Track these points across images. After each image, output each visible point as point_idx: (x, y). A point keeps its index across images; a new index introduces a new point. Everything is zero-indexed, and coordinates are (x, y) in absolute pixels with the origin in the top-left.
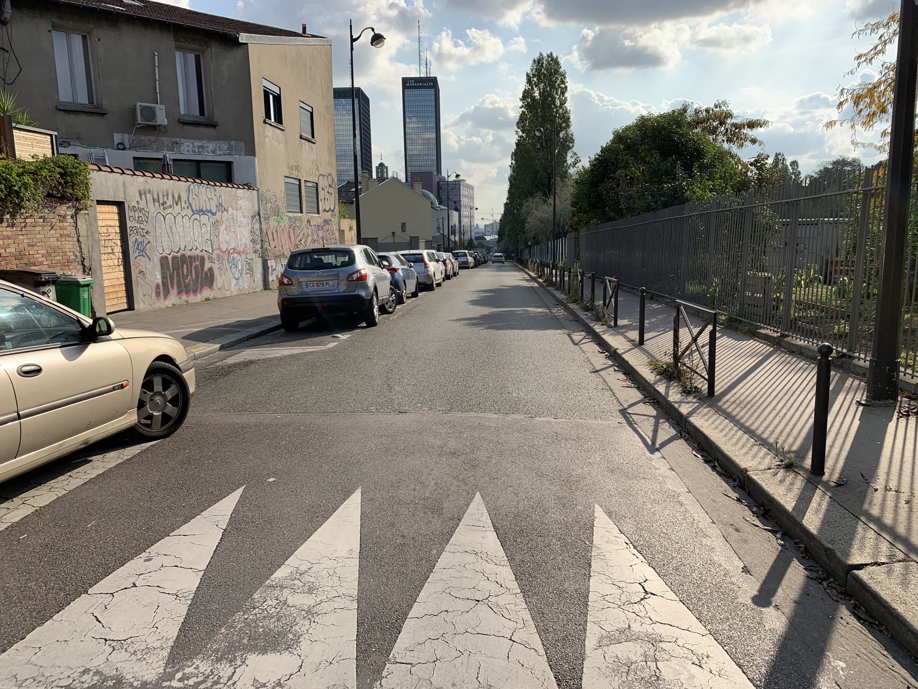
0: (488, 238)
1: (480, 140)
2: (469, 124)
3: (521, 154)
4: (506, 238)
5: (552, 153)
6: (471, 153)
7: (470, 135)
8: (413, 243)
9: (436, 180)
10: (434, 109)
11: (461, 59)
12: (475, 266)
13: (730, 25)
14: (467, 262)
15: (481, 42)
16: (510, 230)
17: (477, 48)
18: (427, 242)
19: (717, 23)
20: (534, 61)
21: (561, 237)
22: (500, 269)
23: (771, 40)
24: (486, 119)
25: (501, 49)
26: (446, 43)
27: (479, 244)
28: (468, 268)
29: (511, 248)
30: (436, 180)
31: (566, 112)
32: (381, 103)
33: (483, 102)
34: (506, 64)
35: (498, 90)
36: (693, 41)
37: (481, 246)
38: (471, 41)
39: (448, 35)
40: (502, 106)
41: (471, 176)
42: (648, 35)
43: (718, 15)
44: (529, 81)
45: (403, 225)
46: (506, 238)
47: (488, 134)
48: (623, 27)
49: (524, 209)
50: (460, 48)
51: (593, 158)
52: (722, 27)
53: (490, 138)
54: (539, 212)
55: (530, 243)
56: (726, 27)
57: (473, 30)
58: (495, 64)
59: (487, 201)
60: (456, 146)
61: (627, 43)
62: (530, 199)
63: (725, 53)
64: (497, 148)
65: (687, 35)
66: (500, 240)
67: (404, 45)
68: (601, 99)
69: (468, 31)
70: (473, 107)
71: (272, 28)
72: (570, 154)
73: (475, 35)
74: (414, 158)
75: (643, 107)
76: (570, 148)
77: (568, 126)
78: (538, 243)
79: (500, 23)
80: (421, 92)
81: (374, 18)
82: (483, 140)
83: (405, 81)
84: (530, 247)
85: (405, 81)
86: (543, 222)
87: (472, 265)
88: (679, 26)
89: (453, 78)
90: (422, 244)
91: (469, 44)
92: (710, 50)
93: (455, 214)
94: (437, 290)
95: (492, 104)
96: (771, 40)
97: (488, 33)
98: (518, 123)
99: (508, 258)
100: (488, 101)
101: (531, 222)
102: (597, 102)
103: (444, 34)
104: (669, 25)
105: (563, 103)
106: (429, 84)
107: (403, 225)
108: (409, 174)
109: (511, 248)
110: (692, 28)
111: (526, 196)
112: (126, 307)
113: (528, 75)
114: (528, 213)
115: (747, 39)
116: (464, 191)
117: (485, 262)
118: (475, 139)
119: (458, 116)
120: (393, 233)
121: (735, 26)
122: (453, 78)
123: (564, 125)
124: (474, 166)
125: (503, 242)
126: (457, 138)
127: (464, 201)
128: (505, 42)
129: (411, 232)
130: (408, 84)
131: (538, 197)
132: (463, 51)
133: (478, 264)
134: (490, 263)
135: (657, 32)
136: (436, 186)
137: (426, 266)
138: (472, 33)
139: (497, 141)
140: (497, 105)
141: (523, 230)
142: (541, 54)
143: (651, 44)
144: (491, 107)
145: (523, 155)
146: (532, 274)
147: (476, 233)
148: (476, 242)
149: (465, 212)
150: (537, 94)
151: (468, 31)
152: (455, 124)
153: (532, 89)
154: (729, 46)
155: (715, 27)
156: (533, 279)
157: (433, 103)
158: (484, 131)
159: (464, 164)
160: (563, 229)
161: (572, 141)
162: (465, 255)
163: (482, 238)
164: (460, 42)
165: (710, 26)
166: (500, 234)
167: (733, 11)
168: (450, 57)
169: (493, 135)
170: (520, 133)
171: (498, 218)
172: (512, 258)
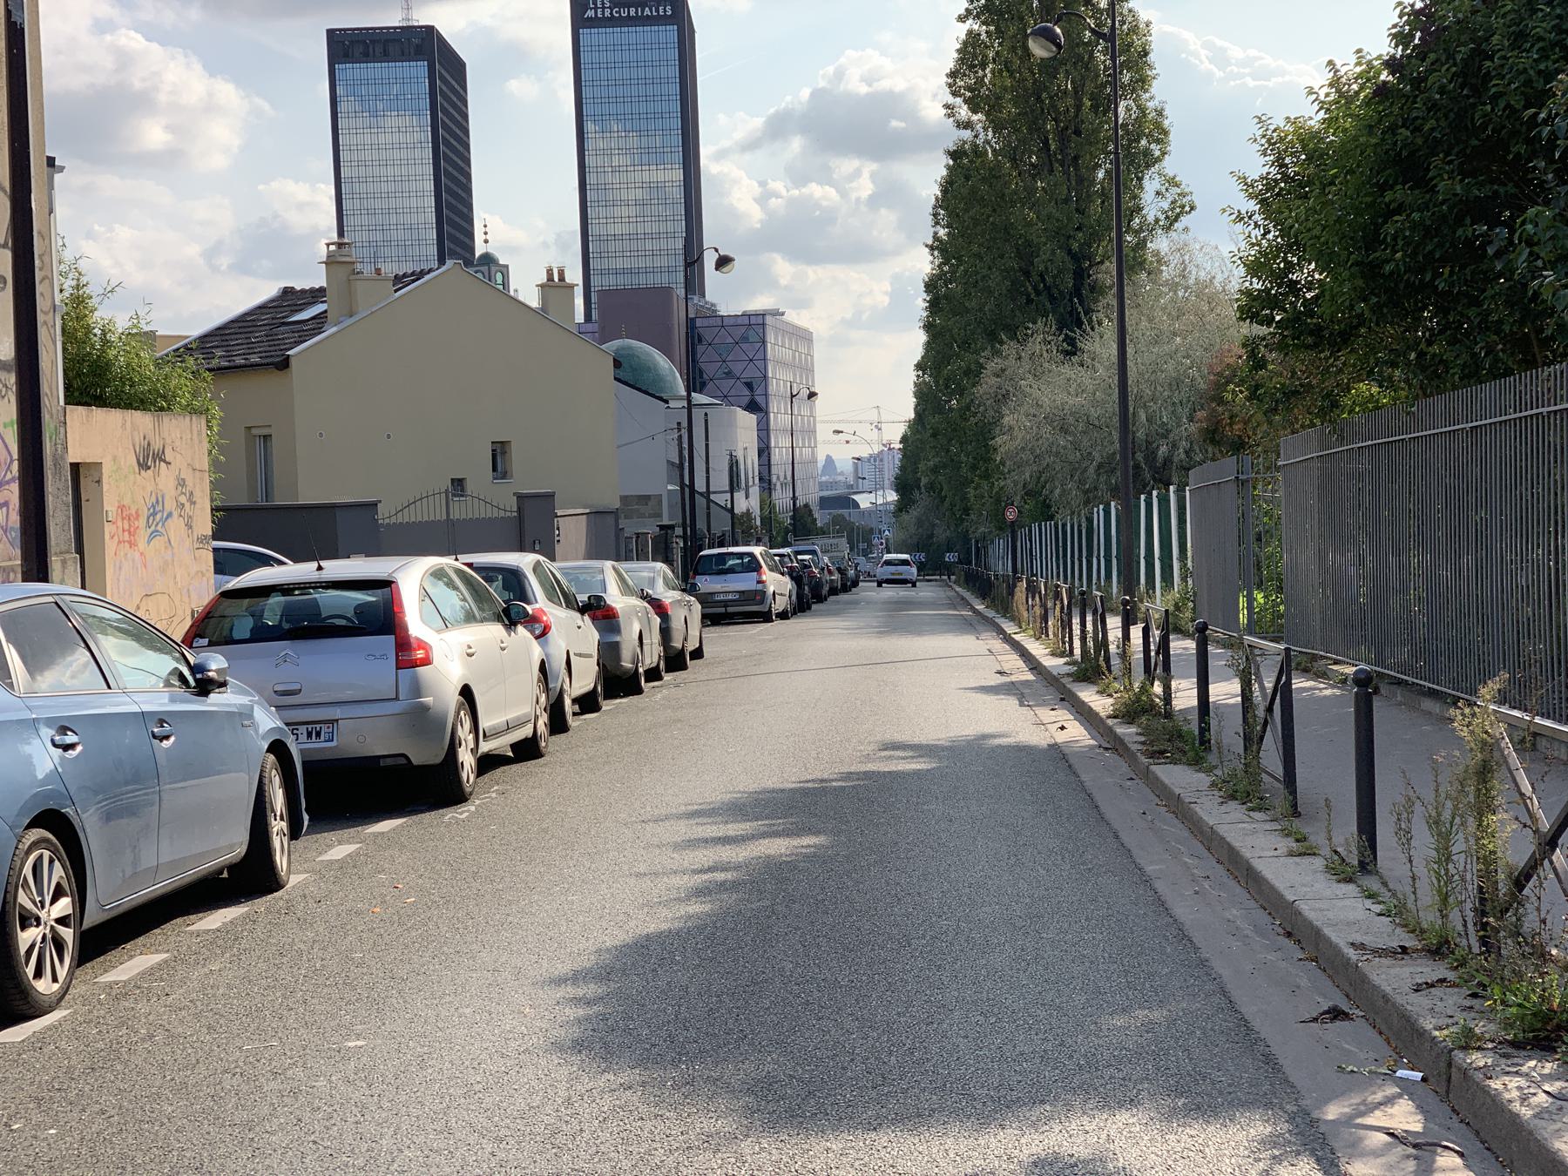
0: (865, 501)
1: (831, 192)
2: (796, 144)
3: (970, 195)
4: (923, 500)
5: (1085, 181)
6: (804, 236)
7: (799, 178)
8: (531, 524)
10: (676, 106)
12: (801, 606)
14: (759, 596)
16: (935, 470)
18: (597, 515)
21: (1144, 488)
22: (897, 620)
24: (845, 128)
27: (837, 520)
28: (766, 617)
29: (942, 534)
32: (514, 85)
33: (840, 75)
37: (842, 527)
40: (899, 85)
41: (803, 304)
45: (499, 452)
46: (923, 500)
47: (857, 173)
49: (988, 384)
51: (1349, 66)
53: (865, 188)
54: (1048, 393)
55: (1011, 515)
62: (1010, 348)
64: (887, 217)
66: (902, 507)
68: (1220, 58)
70: (805, 93)
71: (386, 57)
72: (1151, 184)
74: (612, 246)
76: (1150, 161)
77: (1142, 82)
78: (1045, 512)
82: (843, 194)
86: (1064, 430)
87: (780, 604)
90: (572, 529)
93: (746, 422)
94: (489, 798)
95: (868, 80)
98: (953, 75)
99: (932, 567)
101: (1017, 431)
102: (1207, 65)
107: (499, 452)
108: (594, 298)
109: (942, 534)
111: (993, 337)
112: (82, 655)
114: (1002, 398)
116: (777, 348)
117: (848, 585)
118: (816, 190)
119: (758, 122)
120: (458, 484)
123: (1126, 77)
124: (813, 273)
125: (915, 512)
126: (757, 190)
127: (779, 380)
129: (527, 478)
131: (1041, 338)
133: (811, 596)
134: (867, 591)
136: (674, 330)
137: (408, 655)
139: (887, 194)
140: (885, 85)
141: (984, 460)
144: (864, 89)
145: (973, 202)
146: (1037, 649)
147: (823, 486)
148: (821, 518)
149: (779, 416)
152: (751, 145)
156: (1059, 691)
157: (674, 72)
158: (846, 165)
159: (783, 268)
160: (1151, 455)
161: (1160, 134)
162: (753, 565)
163: (846, 502)
166: (904, 485)
169: (873, 176)
170: (964, 112)
171: (895, 433)
172: (947, 569)
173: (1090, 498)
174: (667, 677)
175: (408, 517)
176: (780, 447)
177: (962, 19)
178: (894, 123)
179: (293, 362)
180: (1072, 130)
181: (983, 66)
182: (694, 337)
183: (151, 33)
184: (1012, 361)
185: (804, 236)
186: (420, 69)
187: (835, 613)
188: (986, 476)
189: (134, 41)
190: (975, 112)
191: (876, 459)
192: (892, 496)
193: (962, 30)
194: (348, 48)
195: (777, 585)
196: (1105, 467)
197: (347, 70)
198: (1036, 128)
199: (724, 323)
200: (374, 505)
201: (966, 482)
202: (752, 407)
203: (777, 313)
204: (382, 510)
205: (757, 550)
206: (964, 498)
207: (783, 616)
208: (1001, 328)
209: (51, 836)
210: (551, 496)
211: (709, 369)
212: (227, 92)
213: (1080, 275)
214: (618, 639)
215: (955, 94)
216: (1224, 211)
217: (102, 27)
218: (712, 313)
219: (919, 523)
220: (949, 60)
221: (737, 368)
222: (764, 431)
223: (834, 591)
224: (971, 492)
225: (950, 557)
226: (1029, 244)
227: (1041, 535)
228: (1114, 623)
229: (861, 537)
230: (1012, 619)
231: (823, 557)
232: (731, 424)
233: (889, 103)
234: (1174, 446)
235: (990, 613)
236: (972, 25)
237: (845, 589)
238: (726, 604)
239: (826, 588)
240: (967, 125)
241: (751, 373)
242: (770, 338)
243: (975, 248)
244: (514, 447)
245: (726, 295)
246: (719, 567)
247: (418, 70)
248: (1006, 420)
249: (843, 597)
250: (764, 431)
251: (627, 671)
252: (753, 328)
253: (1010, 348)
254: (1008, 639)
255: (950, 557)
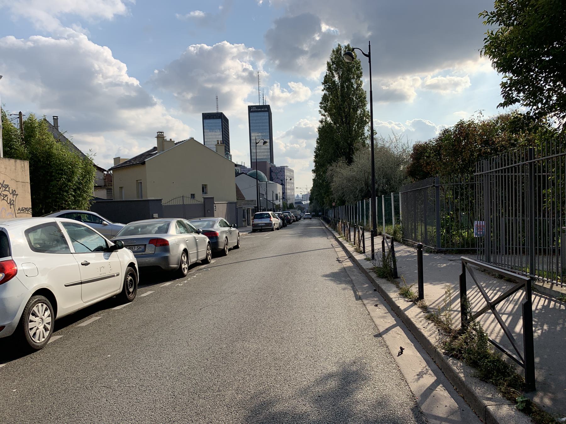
0: (303, 202)
2: (292, 137)
3: (325, 133)
6: (293, 154)
9: (269, 166)
11: (286, 100)
13: (445, 76)
14: (270, 224)
15: (297, 89)
16: (317, 195)
17: (295, 93)
19: (437, 76)
20: (333, 51)
22: (306, 233)
23: (470, 85)
24: (300, 133)
25: (310, 93)
26: (277, 91)
27: (298, 206)
28: (272, 230)
30: (269, 166)
31: (362, 93)
33: (300, 124)
34: (312, 102)
35: (308, 117)
36: (423, 85)
38: (291, 89)
39: (278, 86)
40: (311, 126)
42: (396, 83)
43: (437, 71)
44: (329, 68)
48: (381, 78)
49: (329, 173)
50: (285, 93)
52: (440, 78)
53: (304, 145)
54: (342, 173)
55: (334, 204)
56: (443, 78)
57: (292, 83)
58: (306, 102)
59: (302, 182)
60: (284, 149)
61: (384, 88)
63: (442, 92)
65: (419, 82)
66: (310, 203)
67: (252, 92)
69: (289, 84)
70: (293, 127)
71: (213, 118)
73: (294, 86)
75: (396, 124)
78: (342, 202)
79: (308, 79)
80: (260, 114)
81: (235, 77)
83: (250, 108)
84: (334, 207)
85: (250, 108)
87: (276, 226)
88: (414, 77)
89: (282, 111)
91: (290, 91)
92: (435, 91)
95: (305, 125)
96: (470, 85)
97: (301, 84)
98: (321, 103)
100: (302, 124)
103: (275, 85)
104: (409, 78)
105: (359, 85)
106: (265, 110)
109: (318, 209)
110: (422, 79)
113: (328, 63)
115: (456, 84)
116: (287, 173)
117: (297, 220)
118: (295, 145)
119: (285, 132)
121: (448, 77)
122: (282, 111)
125: (313, 204)
128: (312, 89)
130: (252, 110)
131: (341, 162)
132: (286, 95)
133: (286, 223)
135: (402, 81)
136: (266, 170)
138: (292, 84)
139: (308, 146)
140: (308, 126)
141: (328, 187)
142: (339, 45)
143: (399, 88)
149: (288, 186)
150: (336, 78)
151: (289, 84)
153: (333, 74)
154: (445, 89)
155: (436, 78)
157: (268, 121)
158: (301, 141)
163: (300, 203)
164: (285, 90)
165: (433, 77)
166: (311, 199)
167: (446, 69)
168: (279, 98)
169: (306, 143)
170: (323, 112)
171: (309, 190)
172: (319, 216)
173: (356, 199)
174: (212, 261)
175: (170, 204)
176: (288, 192)
177: (323, 90)
178: (310, 133)
179: (146, 163)
180: (348, 116)
181: (328, 101)
182: (271, 171)
183: (173, 116)
184: (335, 167)
185: (293, 154)
186: (220, 121)
187: (291, 228)
188: (328, 196)
189: (169, 118)
190: (326, 112)
191: (307, 195)
192: (309, 202)
193: (323, 93)
194: (206, 117)
195: (276, 221)
196: (361, 191)
197: (207, 121)
198: (340, 114)
199: (277, 168)
200: (161, 200)
201: (323, 198)
202: (282, 184)
203: (287, 167)
204: (163, 202)
205: (270, 213)
206: (323, 201)
207: (278, 229)
208: (332, 159)
209: (48, 301)
210: (213, 198)
211: (274, 177)
212: (187, 127)
213: (351, 145)
214: (168, 255)
215: (321, 108)
216: (481, 14)
217: (163, 115)
218: (275, 166)
219: (314, 207)
220: (320, 100)
221: (279, 177)
222: (284, 190)
223: (294, 221)
224: (324, 200)
225: (320, 214)
226: (337, 142)
227: (341, 209)
228: (367, 235)
229: (301, 209)
230: (337, 232)
231: (291, 214)
232: (276, 187)
233: (309, 129)
234: (379, 186)
235: (330, 229)
236: (325, 92)
237: (297, 220)
238: (262, 226)
239: (292, 221)
240: (324, 115)
241: (282, 178)
242: (286, 171)
243: (326, 143)
244: (208, 186)
245: (278, 162)
246: (261, 217)
247: (219, 121)
248: (334, 179)
249: (296, 223)
250: (284, 190)
251: (174, 269)
252: (282, 169)
253: (334, 164)
254: (337, 240)
255: (320, 214)
